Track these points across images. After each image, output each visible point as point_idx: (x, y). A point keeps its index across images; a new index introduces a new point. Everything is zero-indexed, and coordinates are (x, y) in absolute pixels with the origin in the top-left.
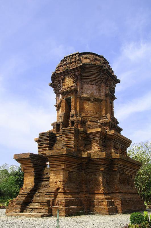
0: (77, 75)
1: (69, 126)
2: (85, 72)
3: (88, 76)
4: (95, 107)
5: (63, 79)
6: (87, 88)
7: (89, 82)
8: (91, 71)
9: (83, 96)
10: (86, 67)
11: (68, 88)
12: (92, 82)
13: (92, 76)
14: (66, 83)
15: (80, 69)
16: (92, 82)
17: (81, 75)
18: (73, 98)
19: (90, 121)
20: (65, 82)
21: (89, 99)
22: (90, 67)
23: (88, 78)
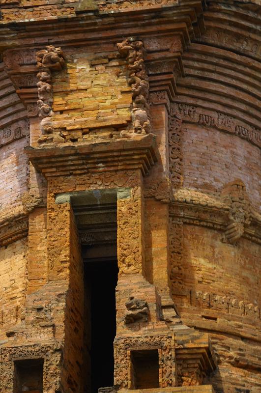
0: (157, 56)
1: (116, 380)
2: (199, 47)
3: (214, 76)
4: (252, 280)
5: (58, 69)
6: (203, 149)
7: (215, 115)
8: (236, 46)
9: (185, 194)
10: (220, 11)
11: (91, 130)
12: (235, 117)
13: (234, 82)
14: (82, 95)
15: (184, 25)
16: (235, 117)
17: (178, 65)
18: (128, 199)
19: (237, 364)
20: (67, 93)
21: (219, 221)
22: (236, 25)
23: (213, 87)
